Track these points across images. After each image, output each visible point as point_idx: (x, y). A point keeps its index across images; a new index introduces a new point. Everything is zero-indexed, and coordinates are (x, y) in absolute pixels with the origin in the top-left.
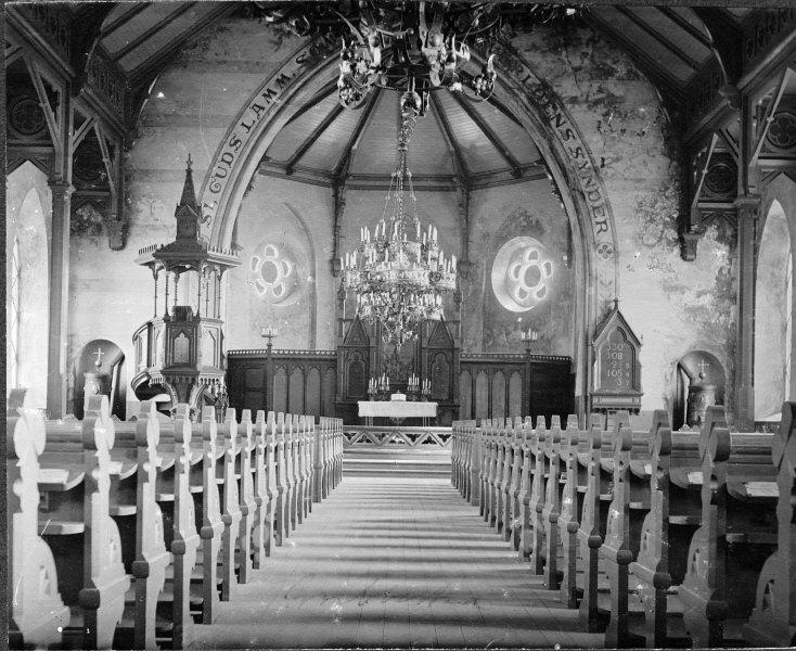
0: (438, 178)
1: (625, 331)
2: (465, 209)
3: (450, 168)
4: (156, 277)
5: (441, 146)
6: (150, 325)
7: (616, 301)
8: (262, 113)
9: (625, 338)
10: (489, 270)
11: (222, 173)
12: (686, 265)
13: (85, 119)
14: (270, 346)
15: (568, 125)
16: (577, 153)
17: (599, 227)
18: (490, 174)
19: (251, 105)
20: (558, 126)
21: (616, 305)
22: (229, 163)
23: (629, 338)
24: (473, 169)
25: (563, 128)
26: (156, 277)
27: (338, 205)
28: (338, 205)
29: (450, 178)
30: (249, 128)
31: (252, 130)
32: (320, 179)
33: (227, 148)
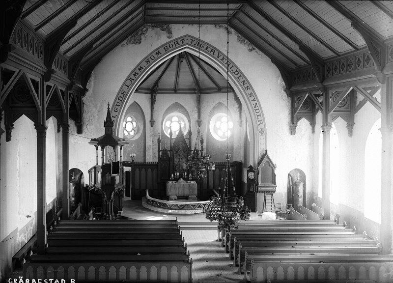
0: (189, 90)
1: (270, 162)
2: (199, 102)
3: (194, 86)
4: (97, 149)
5: (191, 79)
6: (95, 168)
7: (266, 151)
8: (133, 81)
9: (270, 165)
10: (209, 124)
11: (119, 104)
12: (291, 136)
13: (126, 196)
14: (133, 160)
15: (248, 85)
16: (251, 95)
17: (212, 52)
18: (210, 89)
19: (129, 78)
20: (244, 85)
21: (266, 152)
22: (121, 101)
23: (271, 165)
24: (202, 86)
25: (246, 86)
26: (97, 149)
27: (153, 101)
28: (153, 101)
29: (194, 90)
30: (128, 87)
31: (130, 87)
32: (147, 91)
33: (120, 95)
